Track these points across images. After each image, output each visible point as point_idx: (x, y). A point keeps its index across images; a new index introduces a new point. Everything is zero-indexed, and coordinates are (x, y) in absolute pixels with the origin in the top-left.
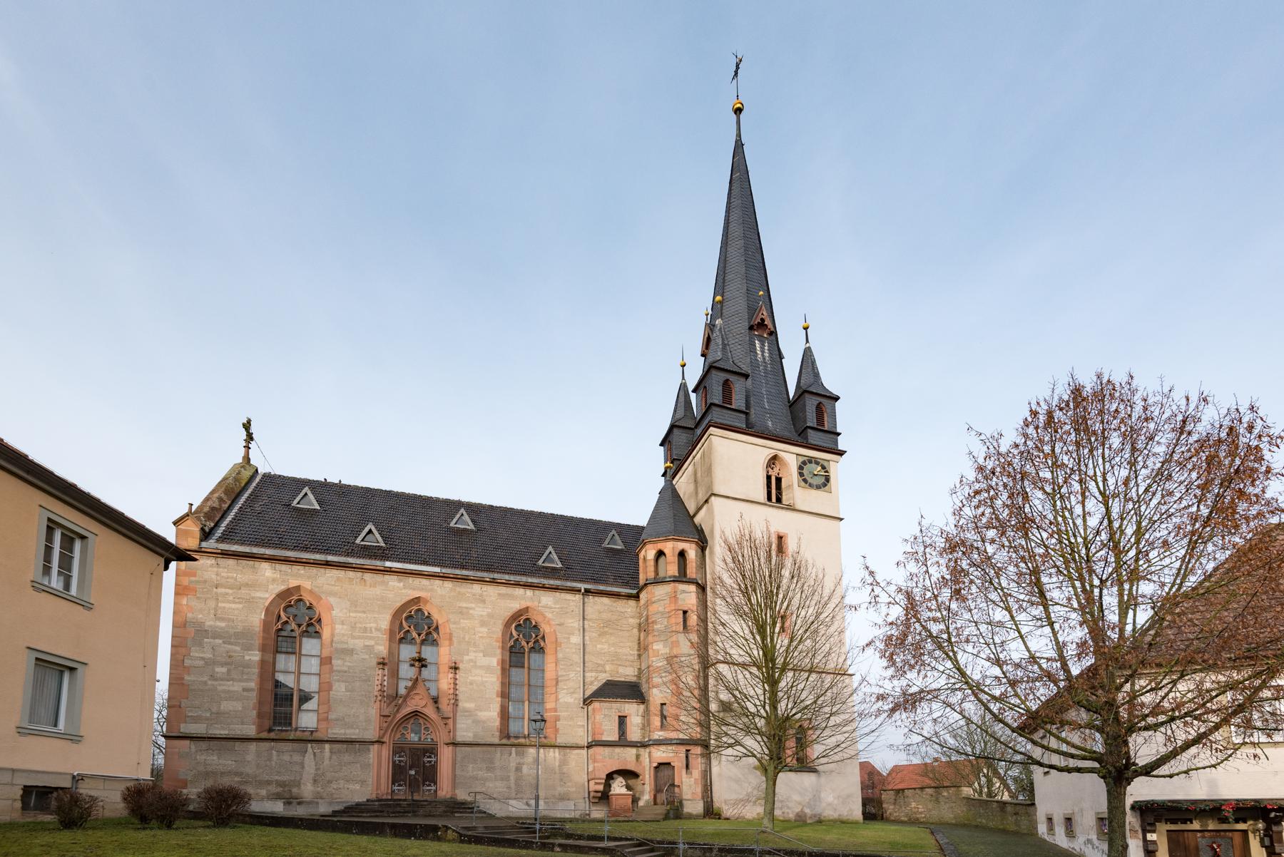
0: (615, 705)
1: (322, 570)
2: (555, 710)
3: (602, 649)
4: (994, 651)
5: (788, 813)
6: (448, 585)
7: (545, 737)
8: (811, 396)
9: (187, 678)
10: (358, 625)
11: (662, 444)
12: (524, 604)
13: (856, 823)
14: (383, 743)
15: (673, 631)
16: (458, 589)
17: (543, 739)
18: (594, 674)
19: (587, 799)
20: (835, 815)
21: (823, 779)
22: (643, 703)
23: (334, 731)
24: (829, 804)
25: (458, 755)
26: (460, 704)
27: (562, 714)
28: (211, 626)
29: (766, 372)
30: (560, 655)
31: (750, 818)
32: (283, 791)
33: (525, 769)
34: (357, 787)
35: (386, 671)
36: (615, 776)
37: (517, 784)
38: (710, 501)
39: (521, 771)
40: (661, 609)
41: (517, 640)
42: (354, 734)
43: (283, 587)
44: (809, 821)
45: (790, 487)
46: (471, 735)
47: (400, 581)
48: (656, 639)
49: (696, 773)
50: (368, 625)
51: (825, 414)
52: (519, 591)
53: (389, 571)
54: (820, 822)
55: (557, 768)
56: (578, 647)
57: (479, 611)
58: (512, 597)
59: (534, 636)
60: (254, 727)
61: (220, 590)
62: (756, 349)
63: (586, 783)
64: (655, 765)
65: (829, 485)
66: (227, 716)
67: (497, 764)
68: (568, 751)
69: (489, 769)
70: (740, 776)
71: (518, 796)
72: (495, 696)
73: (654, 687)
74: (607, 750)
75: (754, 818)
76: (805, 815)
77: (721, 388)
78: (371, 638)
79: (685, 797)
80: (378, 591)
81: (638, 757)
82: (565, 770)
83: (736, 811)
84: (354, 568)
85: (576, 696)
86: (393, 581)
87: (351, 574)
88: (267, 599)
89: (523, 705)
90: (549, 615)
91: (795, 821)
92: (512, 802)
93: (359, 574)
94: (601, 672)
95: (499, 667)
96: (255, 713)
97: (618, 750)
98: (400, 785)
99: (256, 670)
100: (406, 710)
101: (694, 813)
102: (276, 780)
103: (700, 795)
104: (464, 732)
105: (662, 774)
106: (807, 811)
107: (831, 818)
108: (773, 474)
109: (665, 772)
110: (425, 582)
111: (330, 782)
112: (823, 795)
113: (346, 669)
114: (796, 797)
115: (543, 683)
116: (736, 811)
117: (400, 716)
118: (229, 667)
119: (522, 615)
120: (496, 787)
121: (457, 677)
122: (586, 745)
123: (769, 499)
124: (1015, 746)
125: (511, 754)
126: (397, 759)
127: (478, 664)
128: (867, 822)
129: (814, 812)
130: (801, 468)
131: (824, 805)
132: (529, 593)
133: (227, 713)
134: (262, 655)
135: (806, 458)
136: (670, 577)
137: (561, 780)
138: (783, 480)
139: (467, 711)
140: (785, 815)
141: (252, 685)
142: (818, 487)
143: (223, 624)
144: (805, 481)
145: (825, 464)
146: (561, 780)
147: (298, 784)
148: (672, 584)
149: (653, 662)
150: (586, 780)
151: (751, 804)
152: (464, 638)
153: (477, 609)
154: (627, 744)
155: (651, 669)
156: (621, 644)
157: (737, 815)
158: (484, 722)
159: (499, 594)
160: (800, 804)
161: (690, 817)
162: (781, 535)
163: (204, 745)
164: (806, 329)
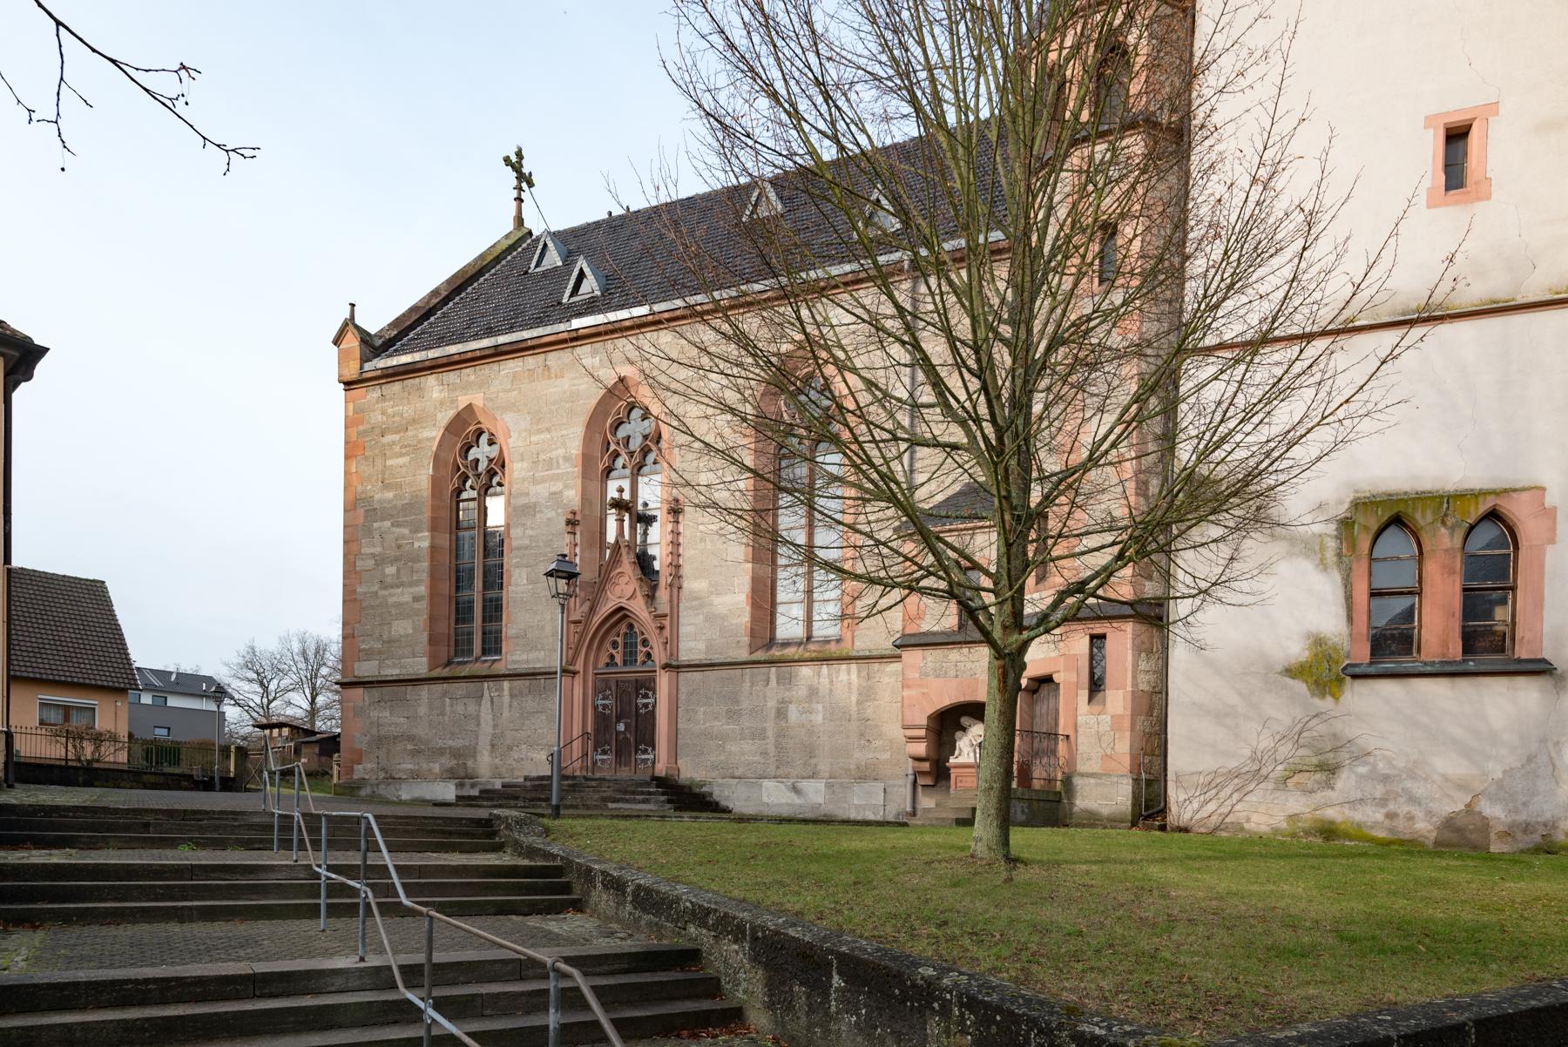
1: (495, 366)
5: (1410, 818)
9: (359, 590)
10: (542, 457)
14: (575, 673)
23: (514, 658)
25: (683, 690)
26: (685, 585)
28: (380, 501)
31: (1264, 829)
32: (458, 765)
33: (793, 713)
35: (578, 536)
36: (965, 721)
37: (777, 746)
39: (786, 718)
42: (539, 660)
43: (451, 413)
46: (702, 646)
49: (1117, 699)
50: (554, 454)
53: (577, 338)
55: (854, 708)
60: (425, 660)
61: (388, 438)
66: (397, 644)
67: (745, 704)
68: (876, 666)
69: (733, 715)
70: (1235, 700)
71: (780, 772)
74: (932, 656)
75: (1276, 831)
76: (1485, 824)
78: (557, 477)
79: (1081, 767)
80: (564, 385)
83: (1211, 807)
84: (533, 348)
87: (532, 361)
88: (434, 438)
92: (768, 784)
96: (426, 634)
98: (604, 752)
99: (425, 565)
100: (605, 609)
101: (1105, 811)
102: (450, 748)
103: (1127, 761)
104: (691, 648)
106: (1494, 811)
111: (510, 748)
113: (527, 542)
114: (1447, 764)
116: (1211, 807)
117: (597, 620)
118: (398, 564)
120: (744, 752)
121: (681, 530)
125: (768, 681)
126: (600, 702)
133: (398, 640)
134: (433, 538)
137: (862, 735)
139: (696, 599)
140: (1400, 824)
141: (422, 589)
143: (389, 495)
146: (862, 735)
147: (472, 752)
151: (1270, 786)
157: (1215, 820)
158: (723, 618)
161: (1092, 820)
163: (376, 693)
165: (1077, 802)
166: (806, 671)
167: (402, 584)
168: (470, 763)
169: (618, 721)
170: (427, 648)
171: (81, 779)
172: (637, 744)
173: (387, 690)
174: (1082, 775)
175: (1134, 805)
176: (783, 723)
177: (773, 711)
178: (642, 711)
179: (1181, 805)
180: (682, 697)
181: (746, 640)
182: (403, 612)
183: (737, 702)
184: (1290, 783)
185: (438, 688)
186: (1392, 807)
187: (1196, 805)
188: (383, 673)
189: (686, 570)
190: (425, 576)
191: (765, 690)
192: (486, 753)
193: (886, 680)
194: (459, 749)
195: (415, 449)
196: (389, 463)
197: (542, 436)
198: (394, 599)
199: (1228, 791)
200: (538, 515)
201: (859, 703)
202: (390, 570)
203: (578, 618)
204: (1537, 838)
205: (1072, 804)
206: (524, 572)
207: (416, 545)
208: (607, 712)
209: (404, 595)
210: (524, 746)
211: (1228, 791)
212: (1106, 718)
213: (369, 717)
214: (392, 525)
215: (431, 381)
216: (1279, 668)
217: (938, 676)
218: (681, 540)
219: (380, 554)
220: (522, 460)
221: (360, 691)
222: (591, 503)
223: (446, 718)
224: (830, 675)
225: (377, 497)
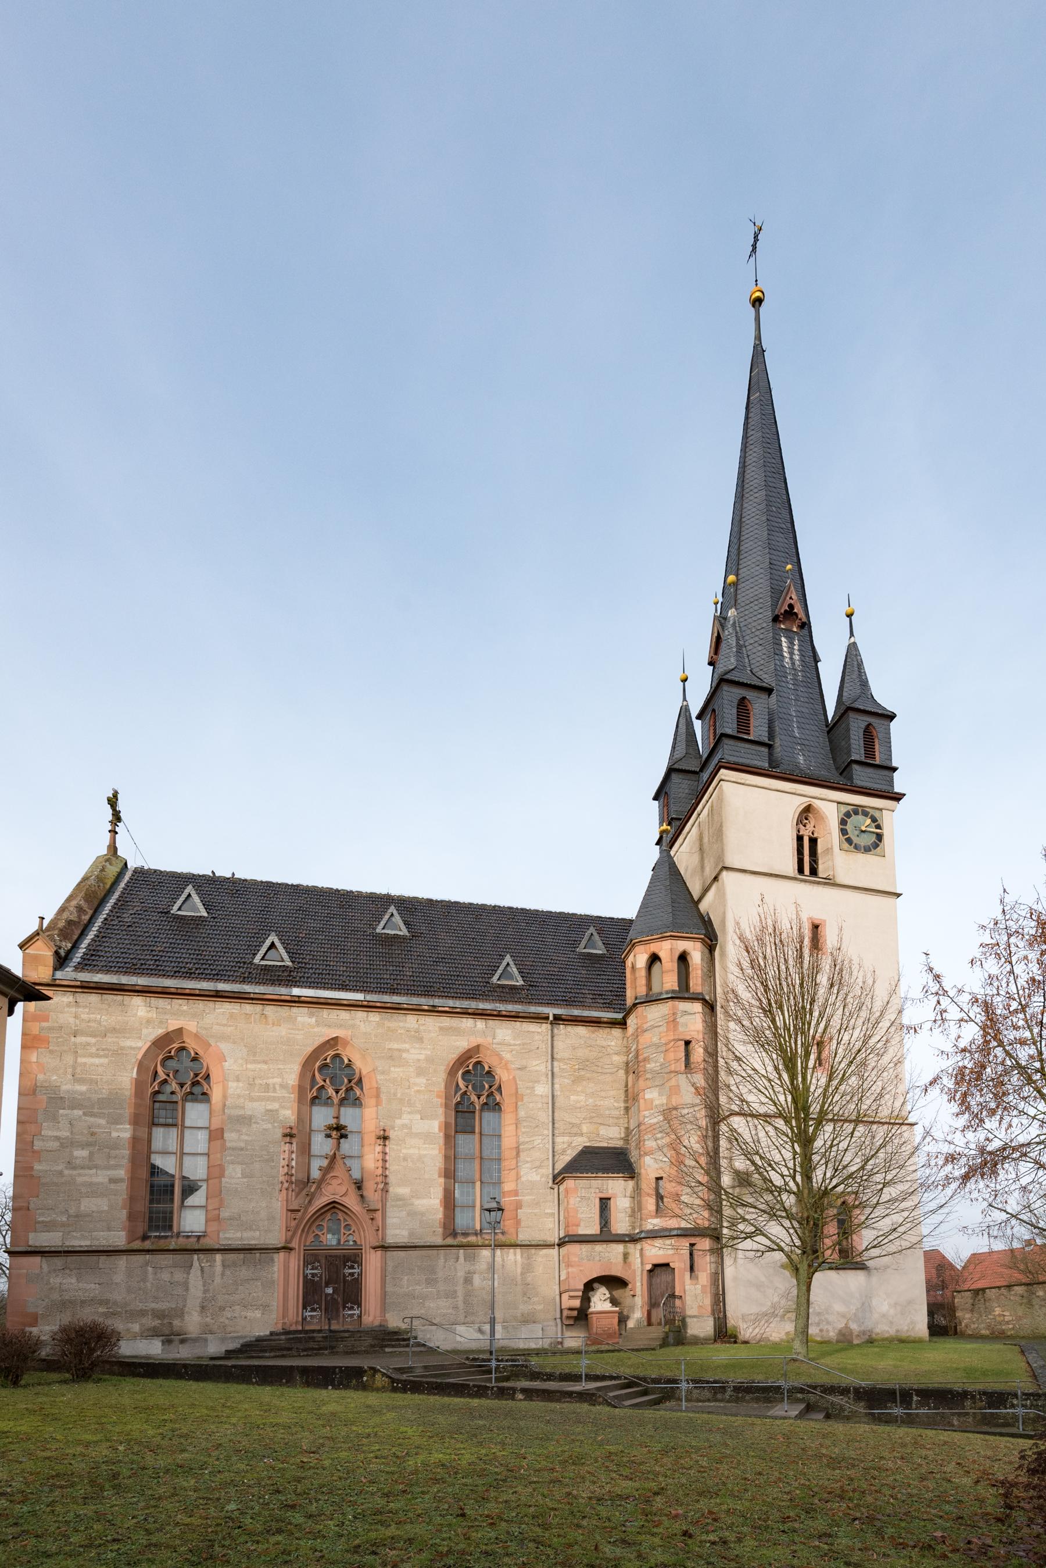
0: (596, 1183)
1: (211, 1004)
2: (516, 1193)
3: (578, 1102)
5: (828, 1331)
6: (374, 1017)
7: (503, 1233)
9: (37, 1167)
11: (655, 798)
12: (474, 1041)
14: (291, 1249)
15: (671, 1072)
16: (387, 1024)
17: (500, 1236)
18: (566, 1139)
19: (559, 1321)
22: (632, 1178)
23: (227, 1235)
24: (884, 1316)
25: (390, 1264)
26: (391, 1189)
27: (526, 1198)
30: (522, 1113)
31: (777, 1339)
33: (477, 1280)
34: (258, 1314)
36: (596, 1285)
38: (720, 877)
39: (471, 1283)
40: (655, 1040)
41: (465, 1093)
42: (254, 1238)
43: (160, 1031)
44: (856, 1342)
45: (829, 850)
46: (405, 1233)
47: (311, 1015)
48: (649, 1083)
49: (704, 1277)
50: (270, 1081)
51: (876, 741)
52: (467, 1023)
53: (298, 1001)
54: (871, 1341)
55: (519, 1277)
56: (544, 1100)
57: (415, 1054)
58: (457, 1032)
59: (487, 1086)
60: (123, 1233)
61: (80, 1039)
62: (782, 650)
63: (558, 1297)
64: (649, 1267)
67: (440, 1274)
68: (533, 1251)
69: (431, 1282)
70: (763, 1279)
71: (468, 1319)
72: (436, 1176)
73: (646, 1154)
74: (585, 1248)
75: (782, 1340)
76: (851, 1332)
77: (735, 711)
79: (689, 1312)
80: (283, 1031)
81: (626, 1256)
83: (757, 1330)
84: (252, 999)
85: (543, 1171)
86: (302, 1016)
87: (248, 1008)
88: (140, 1048)
89: (474, 1188)
90: (507, 1056)
93: (259, 1008)
94: (576, 1135)
95: (442, 1134)
96: (125, 1212)
97: (599, 1248)
99: (126, 1153)
101: (702, 1335)
102: (153, 1310)
103: (709, 1309)
104: (397, 1231)
105: (658, 1281)
106: (854, 1326)
107: (887, 1335)
108: (806, 833)
109: (663, 1277)
110: (344, 1015)
111: (222, 1309)
112: (874, 1302)
113: (242, 1145)
114: (839, 1307)
115: (500, 1153)
117: (312, 1209)
118: (91, 1149)
119: (471, 1057)
122: (557, 1241)
125: (457, 1259)
127: (414, 1130)
129: (862, 1328)
130: (843, 822)
132: (480, 1024)
134: (134, 1130)
136: (667, 992)
137: (525, 1294)
139: (400, 1200)
140: (824, 1333)
141: (122, 1173)
142: (867, 850)
144: (849, 841)
145: (877, 814)
148: (670, 1003)
149: (645, 1117)
150: (557, 1292)
151: (779, 1319)
152: (395, 1094)
153: (412, 1051)
154: (612, 1238)
155: (643, 1127)
156: (603, 1094)
157: (759, 1336)
158: (423, 1214)
159: (441, 1029)
160: (844, 1316)
161: (696, 1341)
162: (817, 922)
163: (58, 1262)
164: (849, 616)
166: (486, 1253)
167: (96, 1167)
168: (176, 1323)
169: (327, 1286)
170: (127, 1224)
171: (254, 1380)
172: (345, 1303)
173: (70, 1259)
176: (469, 1287)
177: (462, 1279)
178: (349, 1278)
179: (745, 1330)
180: (390, 1269)
181: (440, 1230)
182: (95, 1192)
183: (435, 1273)
184: (786, 1317)
185: (140, 1259)
186: (821, 1327)
187: (751, 1330)
188: (67, 1244)
189: (392, 1179)
190: (125, 1162)
191: (458, 1265)
192: (195, 1314)
193: (540, 1259)
194: (164, 1311)
195: (119, 1053)
196: (80, 1060)
197: (259, 1066)
198: (86, 1179)
199: (763, 1322)
200: (254, 1126)
201: (522, 1274)
202: (81, 1153)
203: (296, 1208)
205: (686, 1332)
206: (239, 1169)
207: (114, 1134)
208: (316, 1279)
209: (101, 1177)
210: (237, 1307)
211: (763, 1322)
212: (699, 1287)
213: (48, 1283)
214: (85, 1114)
215: (137, 1001)
216: (779, 1264)
217: (589, 1260)
218: (387, 1158)
219: (67, 1138)
220: (238, 1080)
221: (37, 1259)
222: (303, 1122)
223: (149, 1285)
224: (502, 1255)
225: (64, 1088)
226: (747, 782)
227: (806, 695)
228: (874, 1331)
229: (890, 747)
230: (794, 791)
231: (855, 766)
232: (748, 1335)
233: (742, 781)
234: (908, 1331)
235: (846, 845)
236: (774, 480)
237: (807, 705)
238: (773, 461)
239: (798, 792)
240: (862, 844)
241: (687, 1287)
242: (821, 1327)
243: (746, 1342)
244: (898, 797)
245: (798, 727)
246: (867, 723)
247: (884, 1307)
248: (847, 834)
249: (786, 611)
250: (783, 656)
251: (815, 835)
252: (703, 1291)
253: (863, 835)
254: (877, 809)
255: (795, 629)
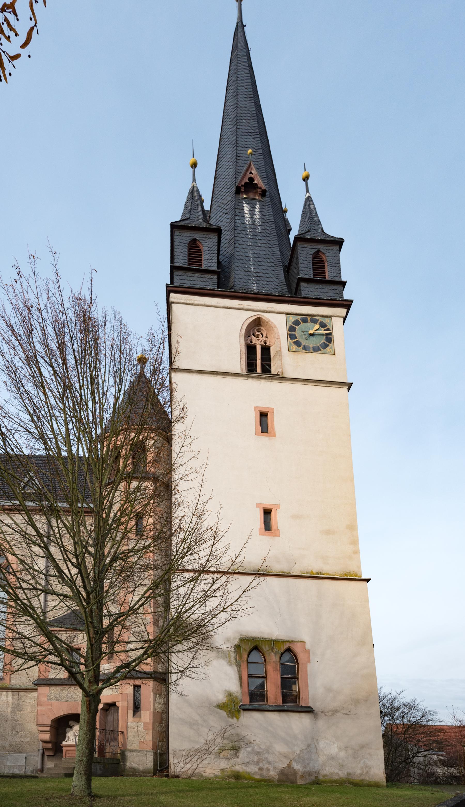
4: (128, 353)
5: (268, 770)
8: (305, 245)
13: (376, 785)
20: (342, 774)
21: (321, 723)
24: (332, 758)
29: (255, 233)
31: (211, 775)
44: (299, 782)
45: (279, 352)
51: (326, 264)
54: (317, 782)
55: (9, 715)
62: (243, 213)
65: (331, 345)
68: (23, 694)
70: (197, 718)
74: (54, 691)
75: (216, 776)
76: (295, 772)
77: (186, 250)
79: (130, 747)
82: (18, 717)
83: (189, 766)
91: (279, 781)
101: (141, 768)
103: (151, 744)
106: (297, 767)
107: (336, 778)
108: (258, 342)
112: (321, 744)
114: (280, 748)
116: (189, 766)
123: (251, 367)
124: (193, 593)
128: (390, 784)
129: (308, 769)
130: (291, 329)
131: (322, 758)
135: (299, 317)
137: (13, 729)
138: (271, 348)
140: (264, 773)
142: (316, 350)
144: (298, 344)
145: (326, 321)
146: (13, 729)
151: (213, 756)
160: (286, 757)
161: (135, 773)
165: (128, 764)
174: (130, 751)
175: (154, 765)
179: (175, 765)
184: (221, 755)
186: (261, 765)
187: (182, 765)
193: (29, 701)
201: (12, 712)
204: (313, 778)
205: (125, 765)
211: (195, 758)
212: (141, 724)
216: (215, 705)
217: (57, 700)
226: (196, 302)
227: (265, 242)
228: (322, 772)
229: (339, 267)
230: (241, 307)
231: (303, 284)
232: (178, 770)
233: (191, 302)
234: (361, 775)
235: (294, 347)
236: (245, 103)
237: (264, 249)
238: (246, 90)
239: (246, 307)
240: (311, 346)
241: (129, 724)
242: (261, 765)
243: (177, 777)
244: (347, 305)
245: (254, 265)
246: (315, 250)
247: (334, 750)
248: (296, 338)
249: (246, 183)
250: (244, 217)
251: (268, 344)
252: (145, 728)
253: (312, 338)
254: (327, 316)
255: (257, 197)
